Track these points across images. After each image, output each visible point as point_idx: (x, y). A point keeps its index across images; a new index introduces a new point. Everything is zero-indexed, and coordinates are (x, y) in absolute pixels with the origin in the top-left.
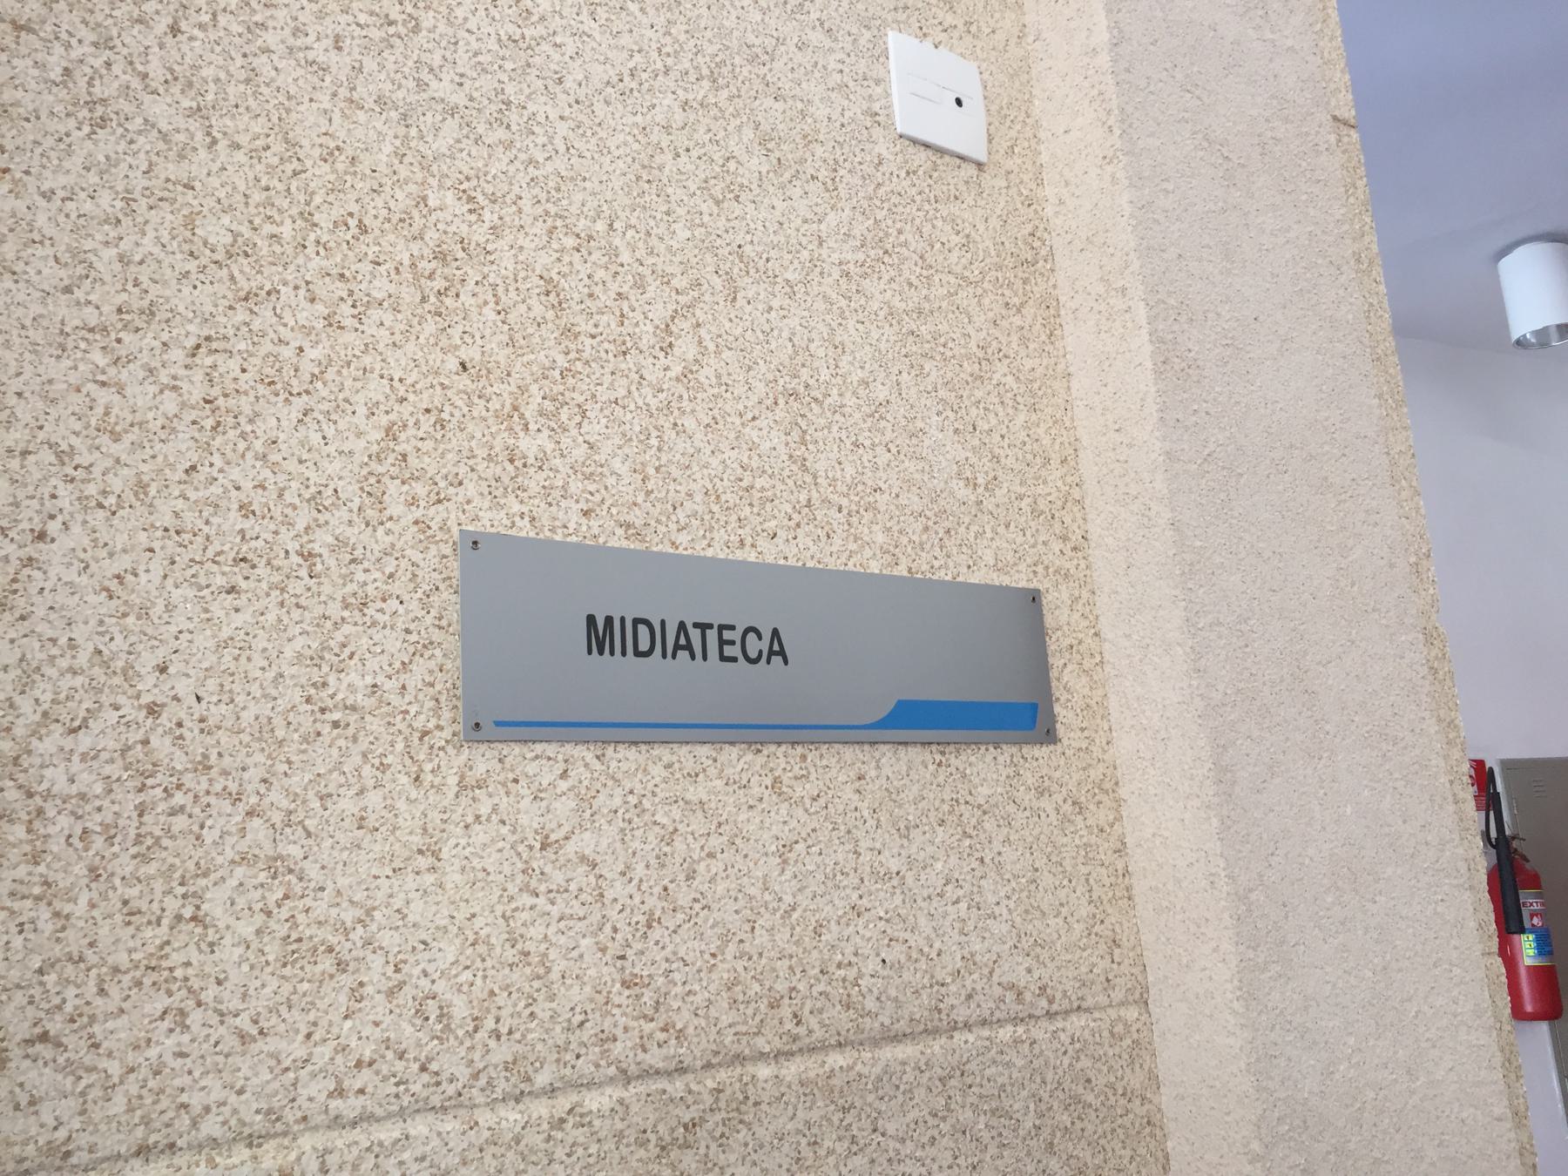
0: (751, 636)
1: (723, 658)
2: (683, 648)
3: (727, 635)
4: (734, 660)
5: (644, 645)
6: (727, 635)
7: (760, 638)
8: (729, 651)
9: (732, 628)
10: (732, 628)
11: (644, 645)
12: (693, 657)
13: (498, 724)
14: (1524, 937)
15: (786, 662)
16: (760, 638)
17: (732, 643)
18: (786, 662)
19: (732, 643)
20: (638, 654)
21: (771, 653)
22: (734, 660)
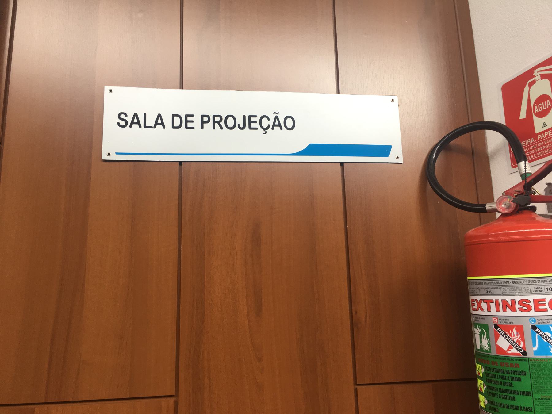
0: (265, 119)
1: (187, 127)
2: (277, 126)
3: (252, 119)
4: (256, 129)
5: (177, 124)
6: (252, 119)
7: (269, 119)
8: (253, 125)
9: (256, 116)
10: (256, 116)
11: (177, 124)
12: (281, 129)
13: (117, 153)
14: (487, 208)
15: (164, 127)
16: (269, 119)
17: (256, 122)
18: (164, 127)
19: (256, 122)
20: (173, 127)
21: (274, 125)
22: (256, 129)
